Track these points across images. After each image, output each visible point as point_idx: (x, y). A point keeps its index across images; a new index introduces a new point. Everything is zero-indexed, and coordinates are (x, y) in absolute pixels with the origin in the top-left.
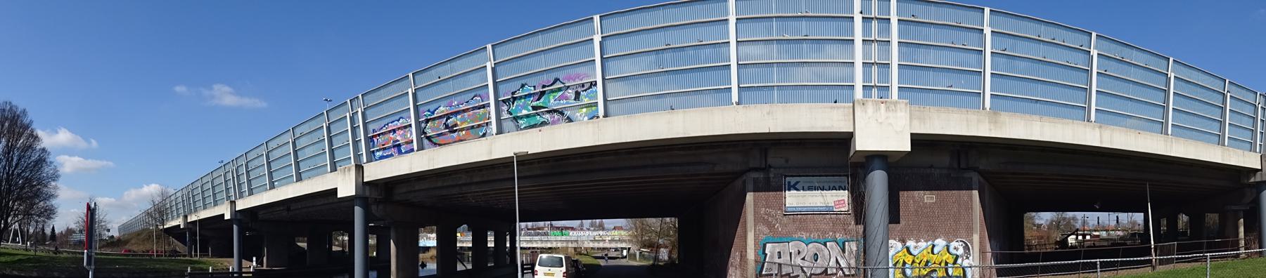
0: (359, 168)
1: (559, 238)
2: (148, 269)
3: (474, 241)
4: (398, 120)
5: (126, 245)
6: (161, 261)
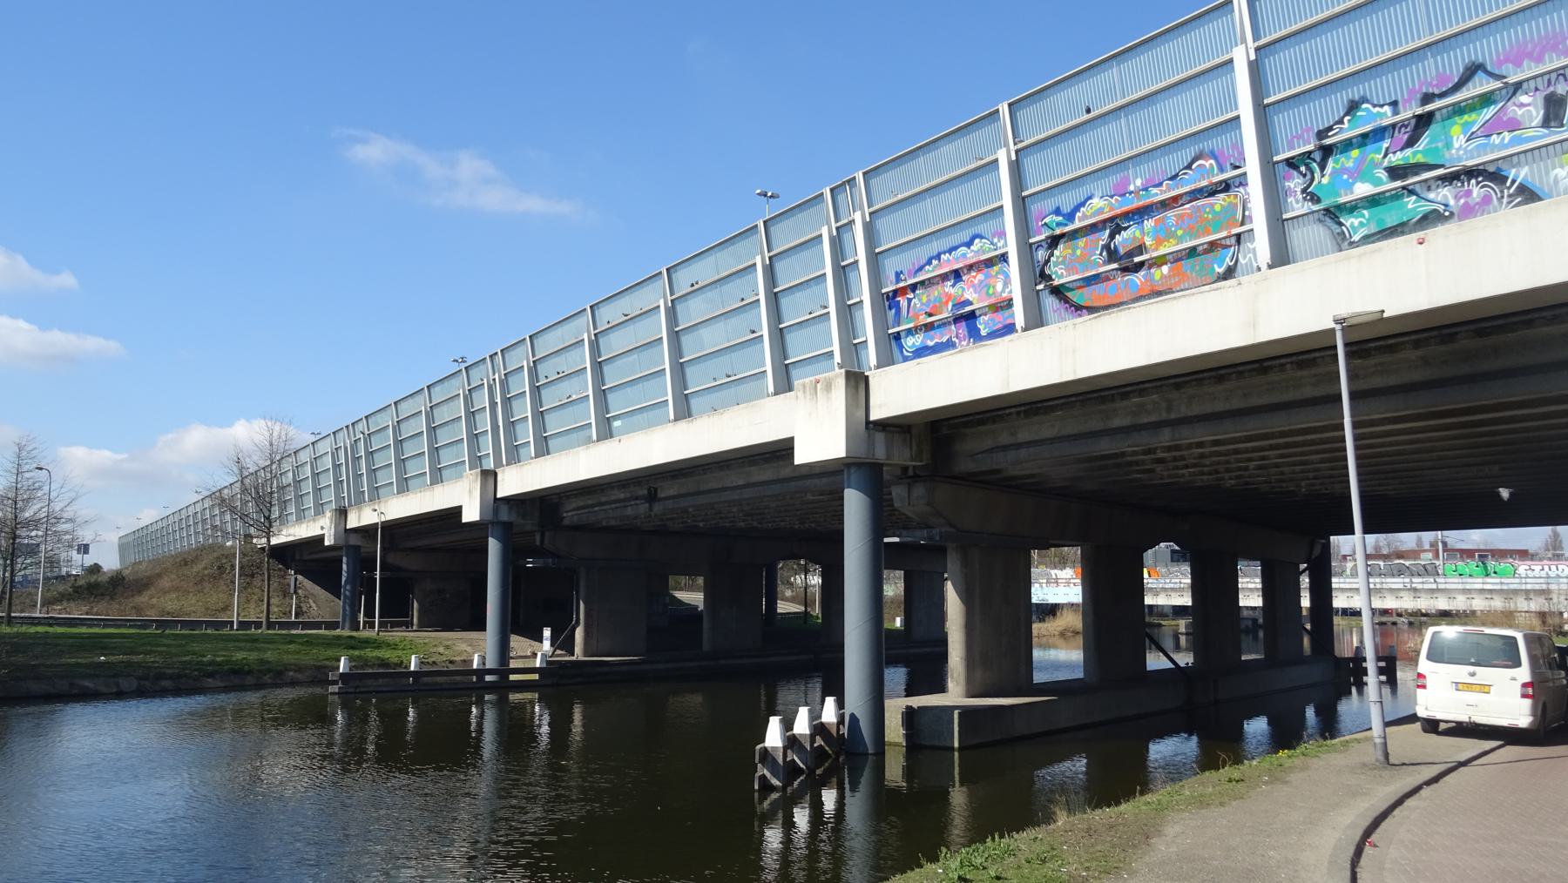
0: (858, 382)
1: (1477, 583)
2: (211, 663)
3: (1196, 588)
4: (969, 244)
5: (140, 592)
6: (254, 640)
